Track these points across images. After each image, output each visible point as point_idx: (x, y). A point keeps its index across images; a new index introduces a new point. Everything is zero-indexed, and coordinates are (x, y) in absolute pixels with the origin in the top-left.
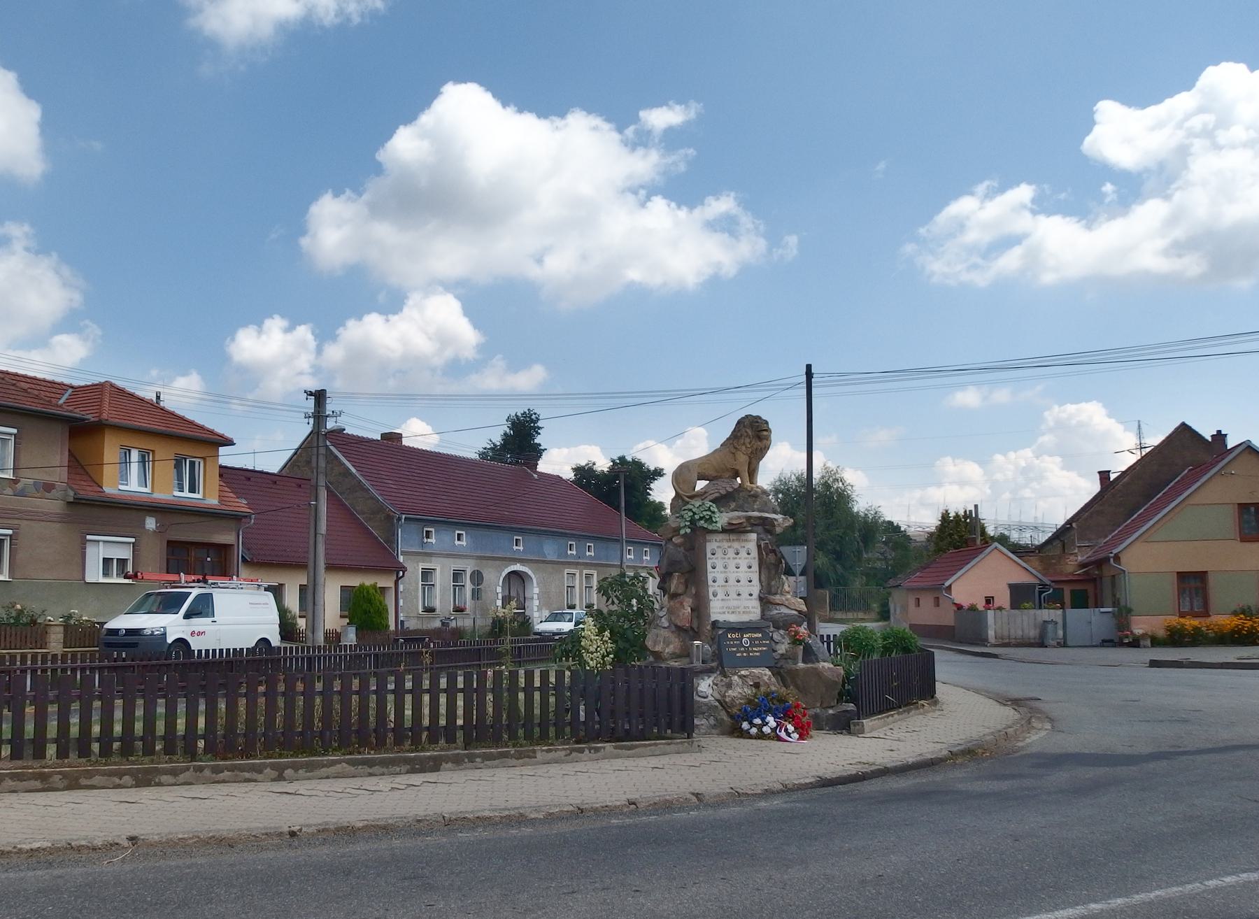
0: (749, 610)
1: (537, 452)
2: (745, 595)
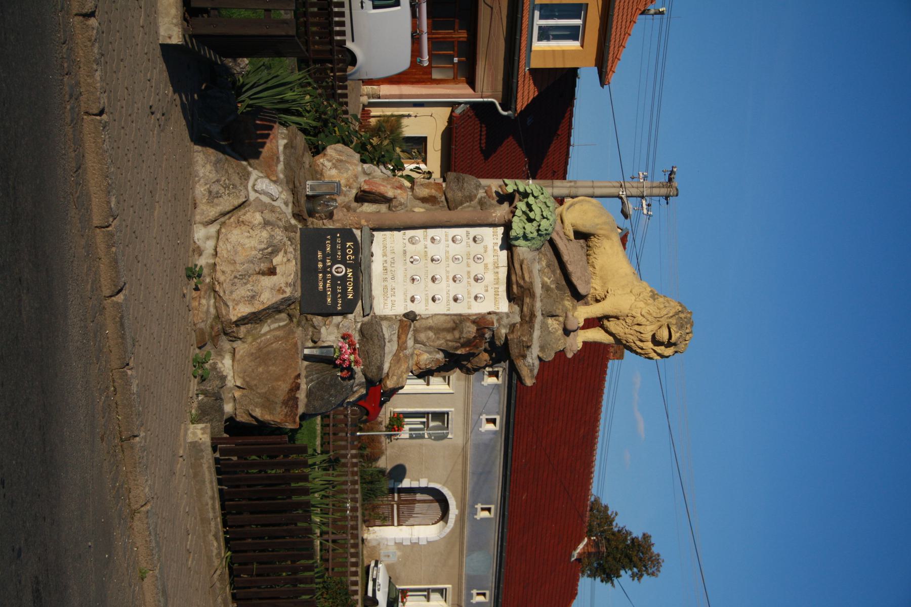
0: (390, 297)
1: (608, 574)
2: (412, 290)
